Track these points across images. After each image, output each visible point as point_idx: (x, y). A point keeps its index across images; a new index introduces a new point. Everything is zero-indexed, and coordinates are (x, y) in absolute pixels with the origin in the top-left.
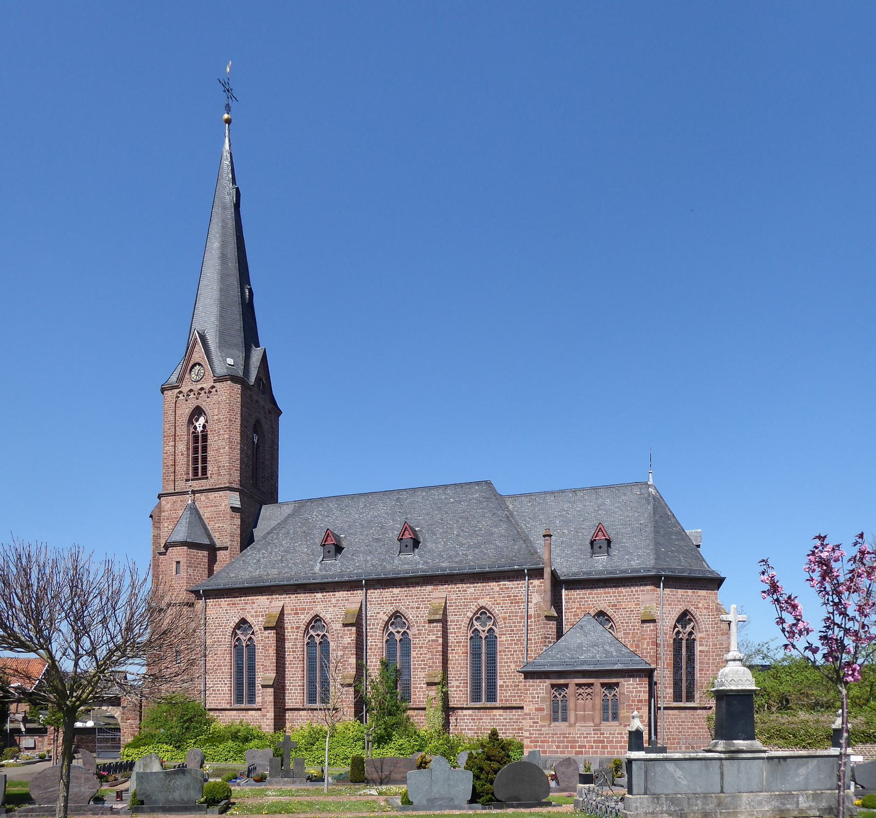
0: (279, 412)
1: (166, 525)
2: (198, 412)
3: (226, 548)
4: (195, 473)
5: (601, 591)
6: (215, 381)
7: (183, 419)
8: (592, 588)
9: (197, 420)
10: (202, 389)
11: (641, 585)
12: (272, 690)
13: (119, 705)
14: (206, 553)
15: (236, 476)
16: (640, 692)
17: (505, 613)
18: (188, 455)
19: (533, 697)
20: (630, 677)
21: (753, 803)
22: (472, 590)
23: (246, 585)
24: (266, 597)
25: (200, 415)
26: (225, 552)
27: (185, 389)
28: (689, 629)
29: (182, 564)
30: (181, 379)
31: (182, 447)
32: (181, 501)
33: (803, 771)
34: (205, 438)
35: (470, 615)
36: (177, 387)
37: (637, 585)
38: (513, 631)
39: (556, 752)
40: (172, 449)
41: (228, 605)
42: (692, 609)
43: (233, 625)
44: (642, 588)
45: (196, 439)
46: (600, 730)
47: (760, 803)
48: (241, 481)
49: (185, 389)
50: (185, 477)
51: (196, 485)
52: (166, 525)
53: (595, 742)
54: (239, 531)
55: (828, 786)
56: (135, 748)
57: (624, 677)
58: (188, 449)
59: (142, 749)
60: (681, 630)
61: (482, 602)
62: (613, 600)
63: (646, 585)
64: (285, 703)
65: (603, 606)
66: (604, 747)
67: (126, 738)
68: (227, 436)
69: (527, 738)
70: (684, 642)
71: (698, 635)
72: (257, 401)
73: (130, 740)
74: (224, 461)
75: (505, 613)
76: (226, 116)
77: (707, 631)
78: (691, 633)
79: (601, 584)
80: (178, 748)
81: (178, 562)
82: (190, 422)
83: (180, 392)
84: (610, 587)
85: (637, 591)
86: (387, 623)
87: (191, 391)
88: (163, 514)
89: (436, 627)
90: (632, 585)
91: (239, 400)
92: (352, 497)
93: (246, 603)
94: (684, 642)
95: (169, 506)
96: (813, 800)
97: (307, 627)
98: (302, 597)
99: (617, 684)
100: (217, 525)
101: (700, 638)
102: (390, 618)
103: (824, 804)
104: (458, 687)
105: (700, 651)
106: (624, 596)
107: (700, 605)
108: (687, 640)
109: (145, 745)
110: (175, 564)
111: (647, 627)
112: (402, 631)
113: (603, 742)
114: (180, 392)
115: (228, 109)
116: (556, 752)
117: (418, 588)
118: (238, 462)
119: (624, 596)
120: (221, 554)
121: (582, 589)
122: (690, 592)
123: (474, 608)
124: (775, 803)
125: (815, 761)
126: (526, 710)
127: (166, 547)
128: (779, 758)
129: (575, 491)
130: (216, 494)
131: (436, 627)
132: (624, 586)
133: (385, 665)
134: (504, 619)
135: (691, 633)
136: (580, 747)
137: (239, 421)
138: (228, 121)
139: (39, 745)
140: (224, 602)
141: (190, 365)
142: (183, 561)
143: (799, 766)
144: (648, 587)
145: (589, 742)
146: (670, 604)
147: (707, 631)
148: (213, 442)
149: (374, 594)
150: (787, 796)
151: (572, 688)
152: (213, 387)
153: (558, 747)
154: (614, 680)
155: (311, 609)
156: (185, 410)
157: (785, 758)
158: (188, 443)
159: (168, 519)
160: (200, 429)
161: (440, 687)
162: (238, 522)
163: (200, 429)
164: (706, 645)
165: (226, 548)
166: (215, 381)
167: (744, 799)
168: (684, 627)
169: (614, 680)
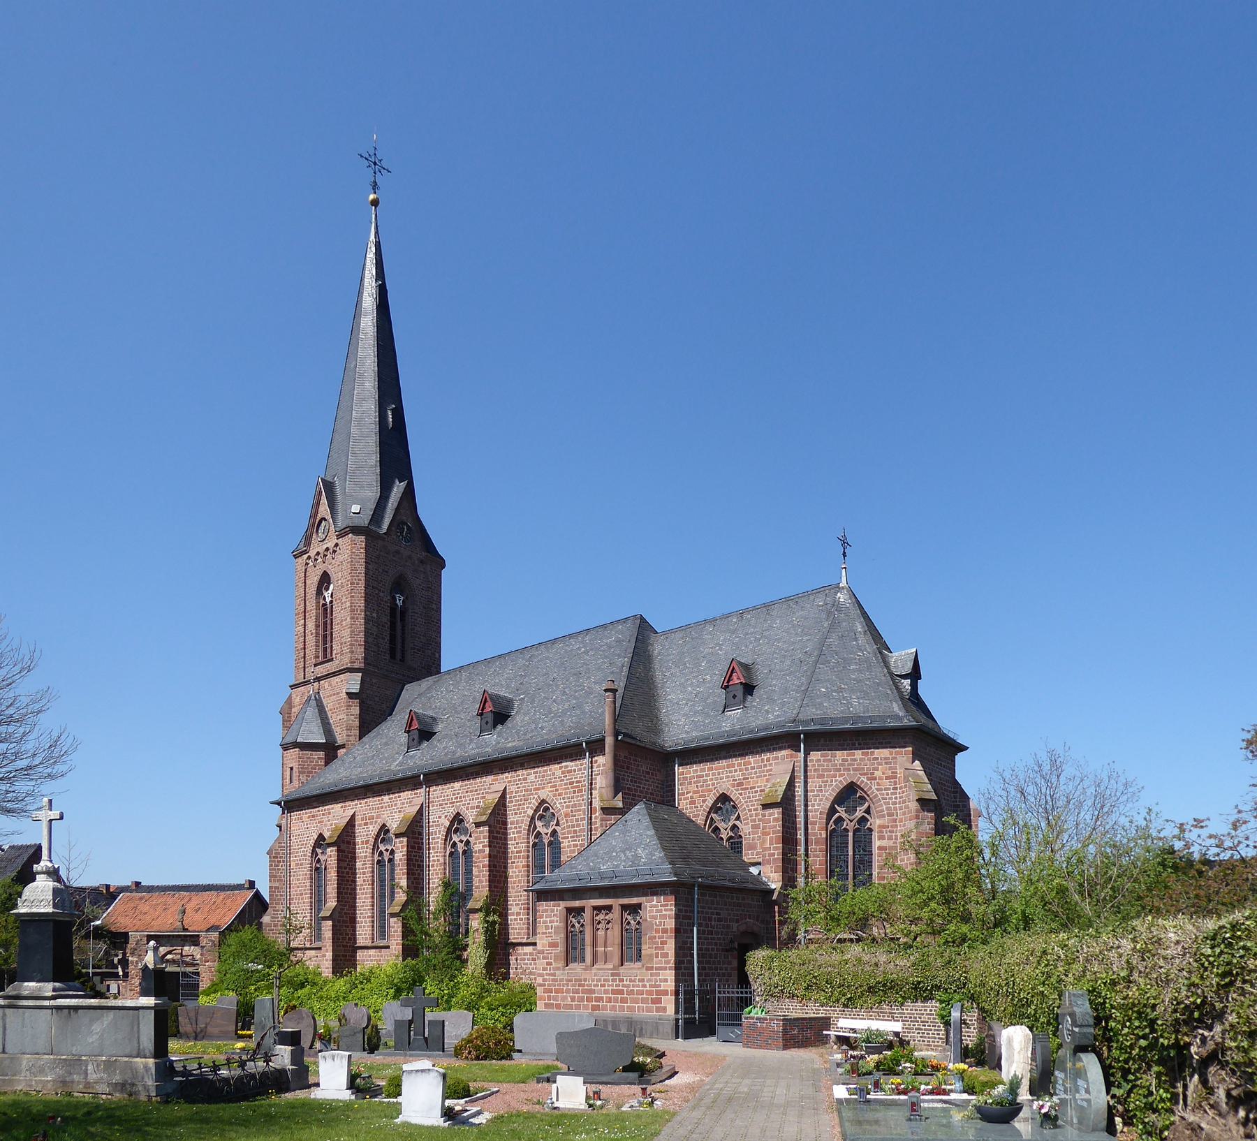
0: (441, 563)
5: (723, 763)
6: (338, 537)
7: (312, 591)
8: (712, 760)
10: (327, 549)
11: (775, 749)
12: (330, 923)
14: (322, 754)
15: (360, 653)
16: (664, 917)
17: (568, 807)
19: (547, 927)
20: (653, 894)
21: (34, 1070)
22: (532, 778)
27: (312, 553)
28: (859, 813)
30: (308, 542)
31: (311, 625)
33: (97, 1028)
35: (530, 812)
36: (305, 552)
37: (769, 751)
38: (575, 832)
39: (571, 1007)
40: (301, 629)
42: (862, 780)
44: (775, 754)
46: (618, 975)
47: (42, 1071)
48: (365, 658)
49: (312, 553)
53: (614, 992)
54: (357, 723)
55: (127, 1051)
57: (645, 895)
60: (844, 815)
61: (543, 794)
62: (738, 776)
63: (781, 749)
64: (355, 939)
65: (725, 786)
66: (624, 1001)
67: (204, 984)
68: (348, 604)
69: (540, 985)
70: (851, 834)
71: (875, 822)
72: (397, 552)
74: (346, 633)
75: (568, 807)
76: (372, 197)
77: (890, 815)
78: (863, 820)
79: (724, 753)
82: (319, 592)
83: (309, 558)
84: (735, 756)
85: (768, 760)
86: (449, 830)
89: (482, 832)
90: (763, 751)
92: (488, 661)
94: (851, 834)
96: (105, 1070)
97: (376, 840)
98: (373, 801)
99: (639, 906)
101: (880, 826)
102: (452, 823)
103: (117, 1078)
104: (518, 914)
105: (880, 848)
106: (753, 768)
107: (877, 774)
108: (855, 831)
111: (770, 815)
112: (465, 839)
113: (621, 992)
116: (571, 1007)
117: (478, 780)
118: (362, 635)
119: (753, 768)
121: (700, 762)
122: (858, 754)
123: (535, 803)
124: (60, 1071)
125: (112, 1013)
126: (539, 947)
128: (69, 1007)
129: (741, 614)
131: (482, 832)
132: (752, 753)
133: (446, 885)
134: (567, 815)
135: (863, 820)
136: (598, 999)
137: (362, 583)
138: (375, 203)
140: (305, 814)
142: (295, 765)
143: (92, 1021)
144: (785, 753)
145: (606, 992)
146: (821, 776)
147: (890, 815)
149: (436, 791)
150: (75, 1063)
151: (587, 915)
152: (337, 545)
153: (573, 999)
154: (634, 900)
155: (378, 817)
156: (314, 580)
157: (76, 1008)
160: (328, 600)
161: (481, 914)
162: (356, 710)
163: (328, 600)
164: (890, 838)
166: (338, 537)
167: (24, 1063)
168: (851, 810)
169: (634, 900)
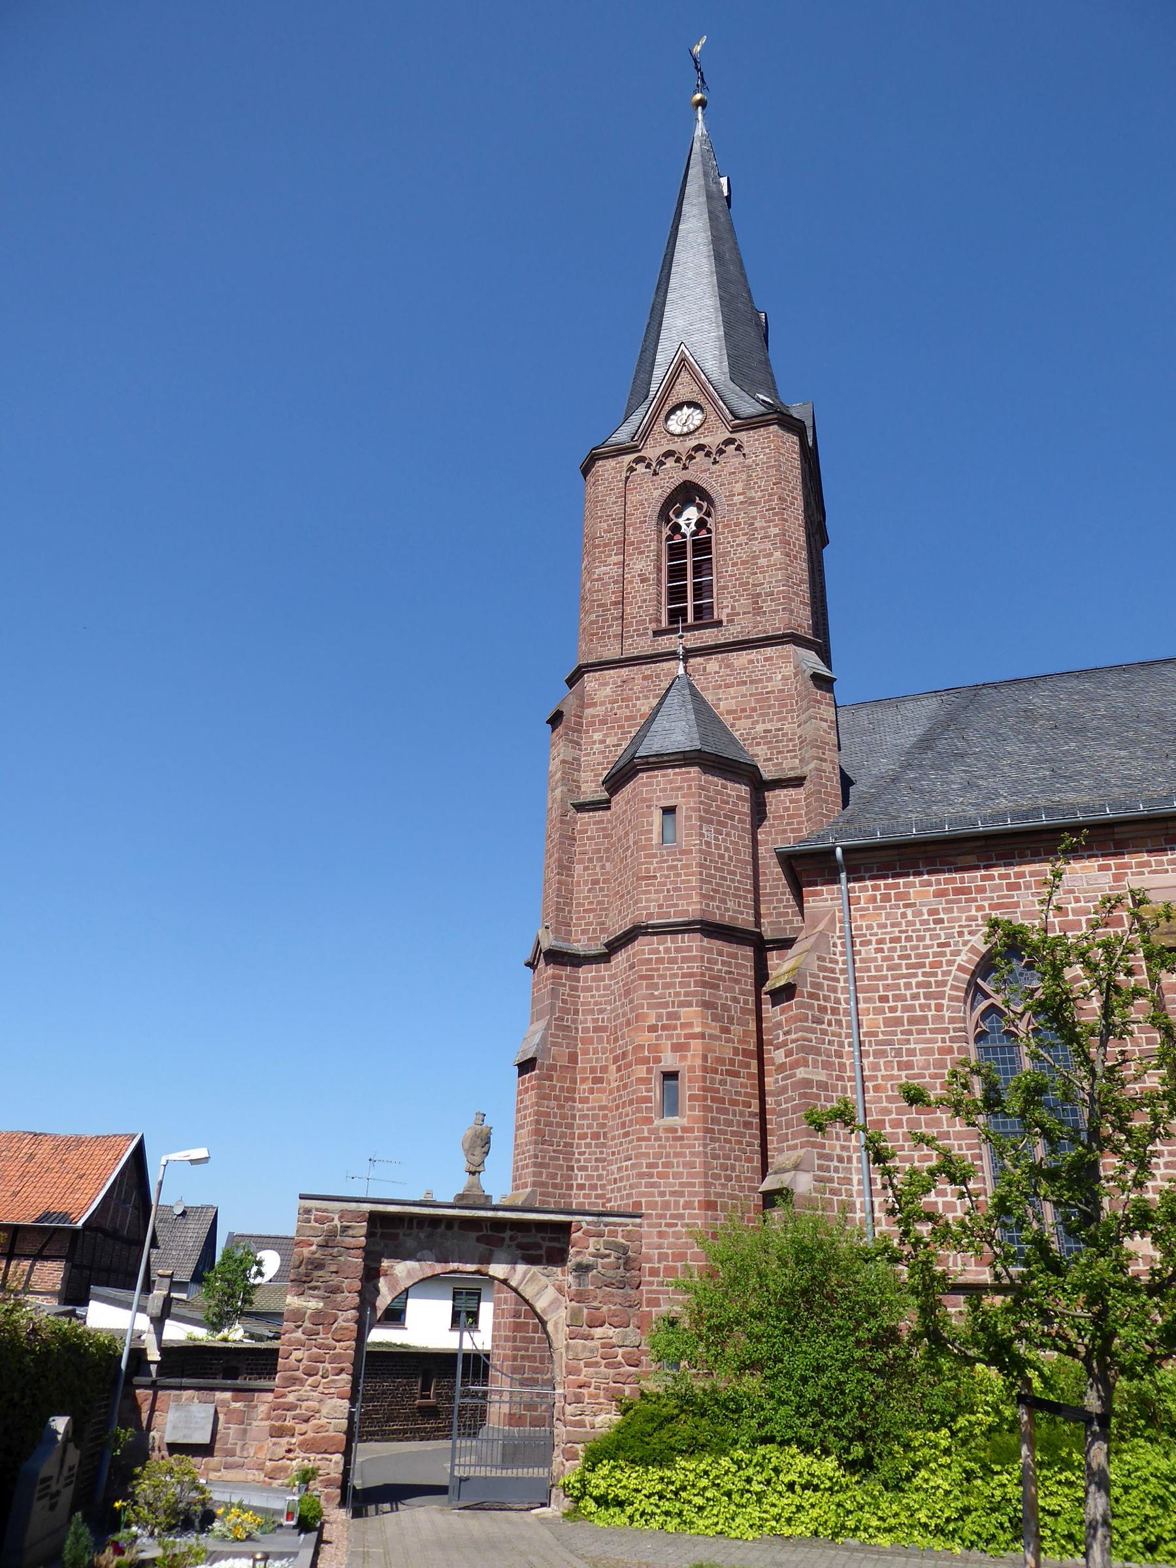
1: (597, 736)
2: (688, 493)
3: (797, 782)
4: (676, 615)
6: (736, 429)
9: (679, 514)
10: (699, 448)
13: (557, 1257)
18: (659, 581)
23: (1010, 824)
24: (1095, 863)
25: (688, 502)
26: (792, 791)
27: (652, 452)
29: (681, 813)
32: (645, 678)
34: (703, 547)
41: (940, 894)
43: (966, 959)
45: (676, 551)
49: (652, 452)
50: (653, 626)
51: (693, 639)
52: (597, 736)
56: (645, 1462)
58: (659, 570)
59: (685, 1468)
73: (606, 1420)
76: (698, 96)
80: (863, 1466)
81: (669, 811)
87: (669, 454)
88: (589, 711)
91: (797, 463)
93: (1016, 887)
95: (608, 690)
100: (760, 728)
109: (694, 1448)
110: (657, 816)
114: (641, 460)
115: (703, 86)
120: (777, 800)
127: (617, 780)
130: (753, 654)
138: (702, 103)
139: (230, 1432)
140: (921, 889)
141: (667, 408)
148: (729, 548)
156: (652, 491)
158: (659, 556)
159: (603, 722)
165: (797, 782)
